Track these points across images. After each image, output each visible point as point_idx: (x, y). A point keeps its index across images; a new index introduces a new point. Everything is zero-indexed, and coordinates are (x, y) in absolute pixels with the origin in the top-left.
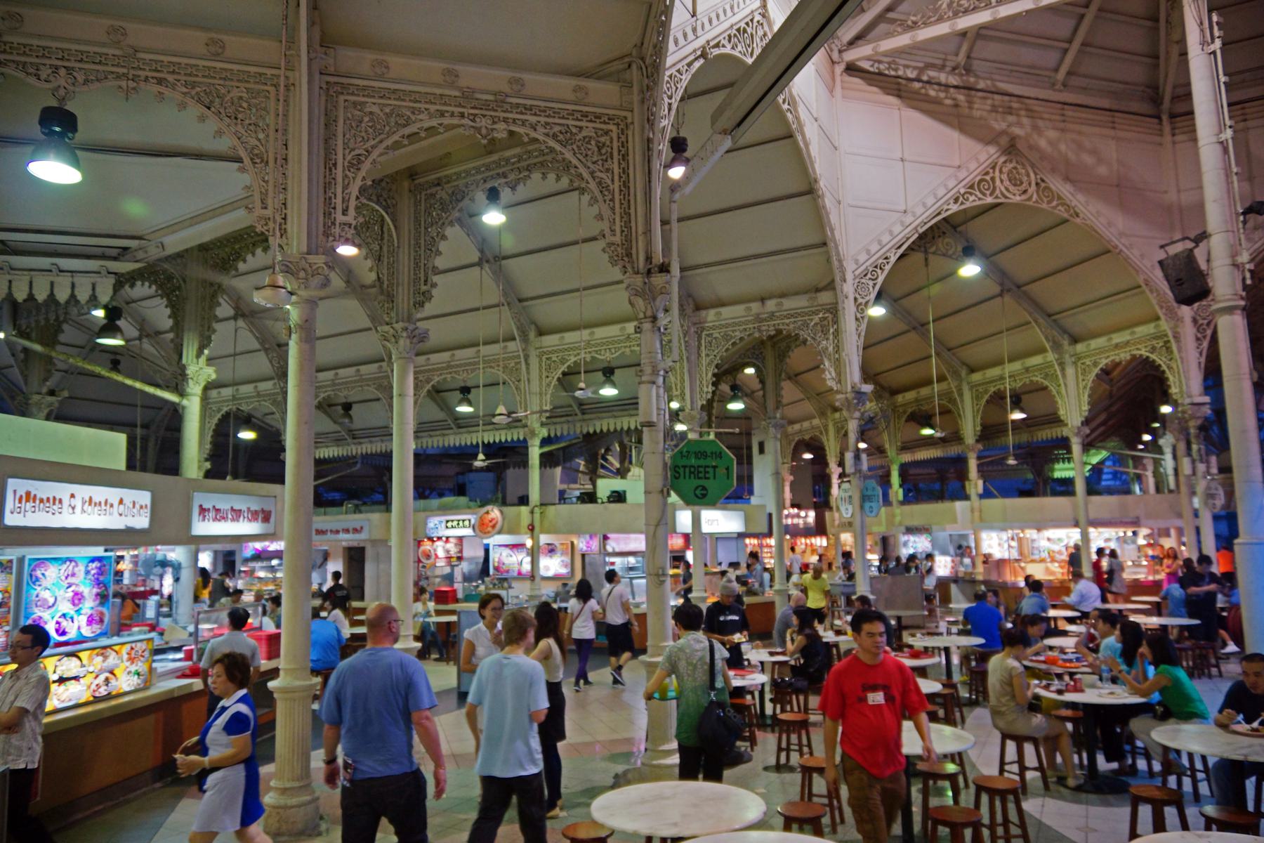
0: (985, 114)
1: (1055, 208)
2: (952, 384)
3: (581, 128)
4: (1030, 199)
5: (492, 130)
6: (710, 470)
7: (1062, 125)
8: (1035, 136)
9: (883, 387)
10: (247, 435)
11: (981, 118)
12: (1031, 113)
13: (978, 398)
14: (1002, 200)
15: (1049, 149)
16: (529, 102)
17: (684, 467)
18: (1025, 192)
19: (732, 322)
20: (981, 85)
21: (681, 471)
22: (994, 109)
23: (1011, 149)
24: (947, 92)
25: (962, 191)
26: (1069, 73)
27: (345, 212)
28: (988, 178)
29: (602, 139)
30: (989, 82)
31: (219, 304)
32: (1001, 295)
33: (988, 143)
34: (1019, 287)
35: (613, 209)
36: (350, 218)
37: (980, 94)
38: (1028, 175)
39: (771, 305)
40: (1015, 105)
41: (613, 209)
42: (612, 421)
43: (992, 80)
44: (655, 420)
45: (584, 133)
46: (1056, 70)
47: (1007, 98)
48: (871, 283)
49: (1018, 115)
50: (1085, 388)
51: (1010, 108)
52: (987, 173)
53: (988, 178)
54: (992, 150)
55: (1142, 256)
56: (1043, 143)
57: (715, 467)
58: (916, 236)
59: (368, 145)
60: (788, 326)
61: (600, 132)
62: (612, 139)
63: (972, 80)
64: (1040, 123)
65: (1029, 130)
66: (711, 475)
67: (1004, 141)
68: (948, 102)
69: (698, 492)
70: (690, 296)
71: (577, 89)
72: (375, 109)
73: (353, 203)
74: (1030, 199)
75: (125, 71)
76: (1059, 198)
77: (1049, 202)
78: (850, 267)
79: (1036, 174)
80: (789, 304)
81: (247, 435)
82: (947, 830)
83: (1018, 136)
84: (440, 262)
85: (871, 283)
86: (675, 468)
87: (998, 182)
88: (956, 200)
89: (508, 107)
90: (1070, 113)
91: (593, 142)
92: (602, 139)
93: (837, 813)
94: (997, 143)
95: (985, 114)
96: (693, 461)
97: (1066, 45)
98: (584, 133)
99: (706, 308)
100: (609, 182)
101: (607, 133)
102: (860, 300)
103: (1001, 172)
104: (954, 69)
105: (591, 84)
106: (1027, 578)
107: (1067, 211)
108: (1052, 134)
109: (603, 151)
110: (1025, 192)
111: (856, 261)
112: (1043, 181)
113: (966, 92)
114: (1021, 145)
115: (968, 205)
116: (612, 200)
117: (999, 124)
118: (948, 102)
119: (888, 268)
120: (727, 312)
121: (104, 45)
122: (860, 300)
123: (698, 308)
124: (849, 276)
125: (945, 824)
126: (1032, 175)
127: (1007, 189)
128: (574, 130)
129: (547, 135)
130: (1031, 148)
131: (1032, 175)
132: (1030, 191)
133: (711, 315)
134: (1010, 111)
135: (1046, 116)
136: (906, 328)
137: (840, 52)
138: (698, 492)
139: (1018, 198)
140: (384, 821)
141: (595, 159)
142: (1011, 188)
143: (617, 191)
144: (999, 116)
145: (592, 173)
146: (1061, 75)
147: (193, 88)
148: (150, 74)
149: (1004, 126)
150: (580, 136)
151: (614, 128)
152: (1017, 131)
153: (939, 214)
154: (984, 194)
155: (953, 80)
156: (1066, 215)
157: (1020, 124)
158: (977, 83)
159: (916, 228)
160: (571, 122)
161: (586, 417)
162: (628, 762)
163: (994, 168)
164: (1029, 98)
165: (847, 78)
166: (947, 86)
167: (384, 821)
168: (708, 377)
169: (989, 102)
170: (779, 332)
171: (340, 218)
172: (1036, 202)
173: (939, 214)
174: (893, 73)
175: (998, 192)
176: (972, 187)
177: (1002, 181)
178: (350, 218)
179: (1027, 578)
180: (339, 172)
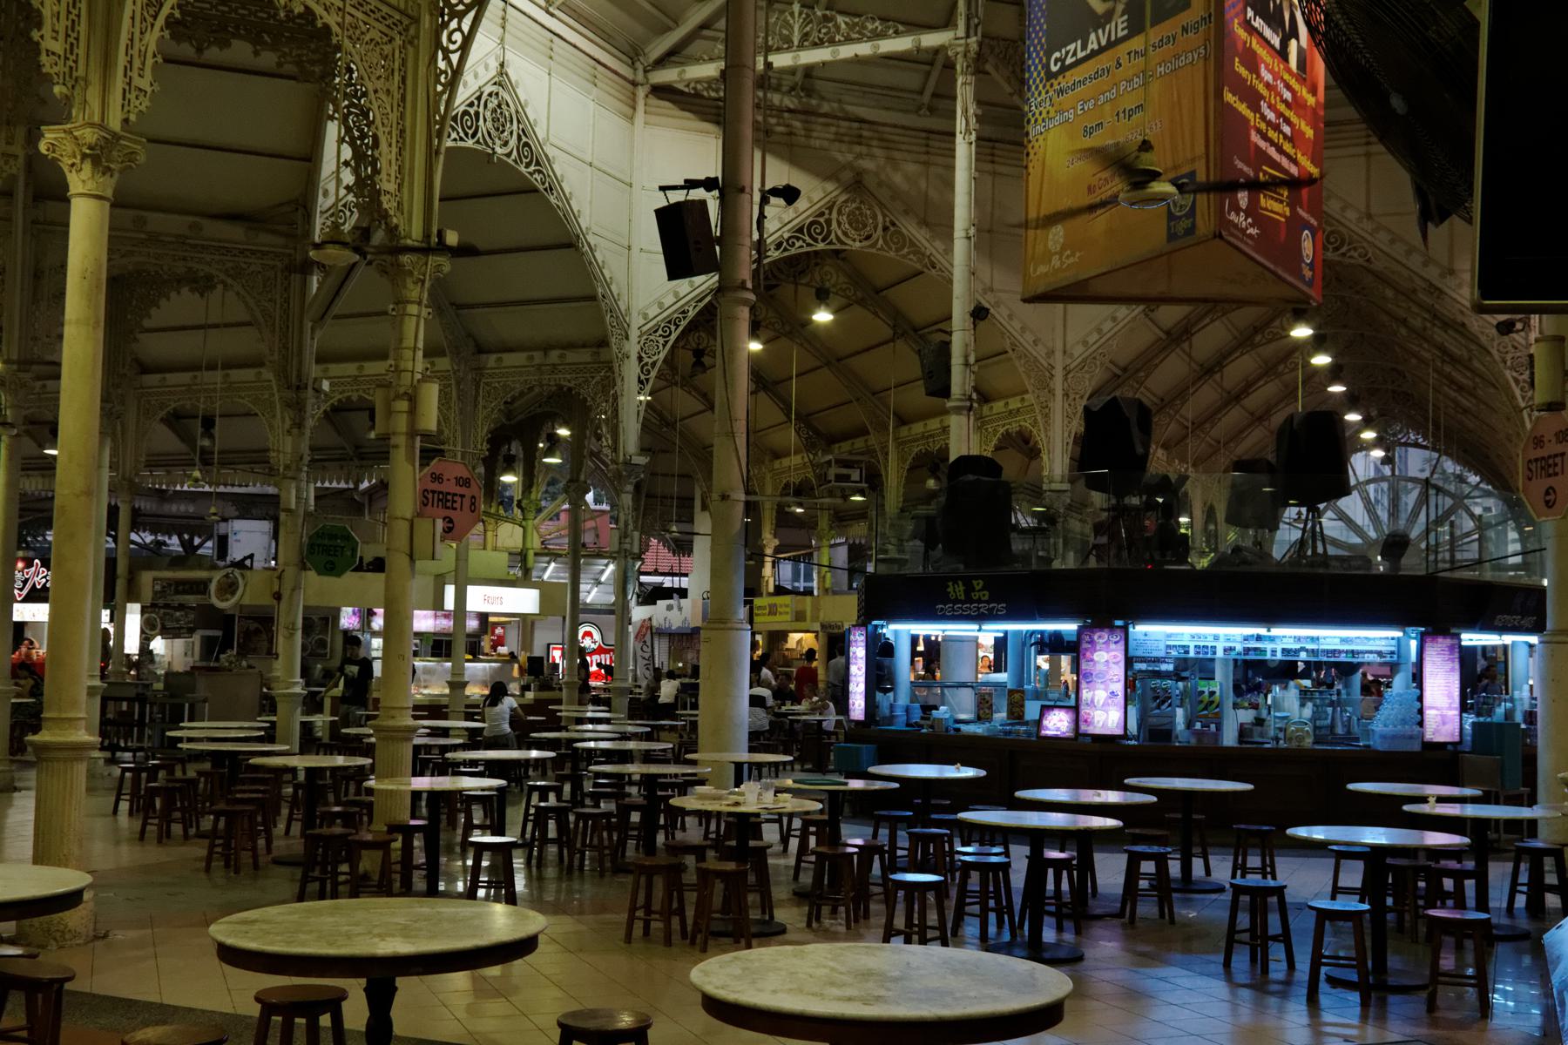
0: (826, 144)
1: (904, 256)
2: (873, 440)
4: (874, 245)
7: (924, 158)
8: (889, 169)
9: (817, 433)
11: (822, 149)
12: (887, 144)
13: (902, 459)
14: (838, 246)
15: (905, 186)
18: (868, 238)
19: (512, 370)
20: (826, 108)
22: (839, 138)
23: (857, 185)
24: (778, 117)
25: (786, 236)
26: (934, 95)
28: (822, 220)
30: (835, 105)
32: (892, 340)
33: (827, 178)
34: (916, 330)
37: (821, 120)
38: (874, 217)
39: (554, 356)
40: (865, 133)
43: (840, 101)
44: (293, 506)
46: (921, 93)
47: (856, 125)
48: (661, 341)
49: (869, 146)
51: (860, 136)
52: (822, 214)
54: (830, 186)
55: (1010, 317)
56: (898, 179)
60: (566, 379)
63: (814, 102)
64: (897, 155)
65: (882, 161)
67: (847, 176)
68: (780, 129)
70: (469, 335)
71: (192, 226)
74: (874, 245)
76: (912, 244)
77: (897, 250)
78: (636, 321)
79: (884, 216)
80: (572, 357)
83: (865, 171)
84: (147, 323)
85: (661, 341)
86: (311, 546)
87: (834, 225)
90: (937, 144)
94: (838, 180)
95: (826, 144)
96: (326, 542)
97: (927, 68)
99: (490, 352)
102: (646, 360)
103: (840, 212)
104: (793, 89)
105: (205, 222)
106: (1302, 705)
107: (920, 261)
108: (912, 168)
110: (868, 238)
111: (645, 316)
112: (894, 224)
113: (803, 117)
114: (870, 182)
115: (793, 251)
117: (843, 155)
118: (780, 129)
119: (684, 323)
120: (511, 359)
122: (646, 360)
123: (481, 350)
124: (634, 334)
126: (880, 218)
127: (845, 234)
130: (880, 184)
131: (880, 218)
132: (875, 236)
133: (491, 360)
134: (859, 140)
135: (904, 147)
136: (818, 363)
137: (646, 71)
139: (858, 244)
142: (852, 232)
144: (844, 147)
146: (926, 98)
149: (850, 157)
152: (867, 164)
154: (816, 240)
155: (789, 102)
156: (918, 266)
157: (872, 157)
158: (819, 106)
161: (364, 463)
163: (830, 209)
164: (884, 125)
165: (653, 101)
166: (781, 110)
168: (482, 431)
169: (833, 129)
170: (560, 387)
172: (882, 249)
174: (713, 94)
175: (833, 236)
176: (800, 230)
177: (839, 224)
179: (1302, 705)
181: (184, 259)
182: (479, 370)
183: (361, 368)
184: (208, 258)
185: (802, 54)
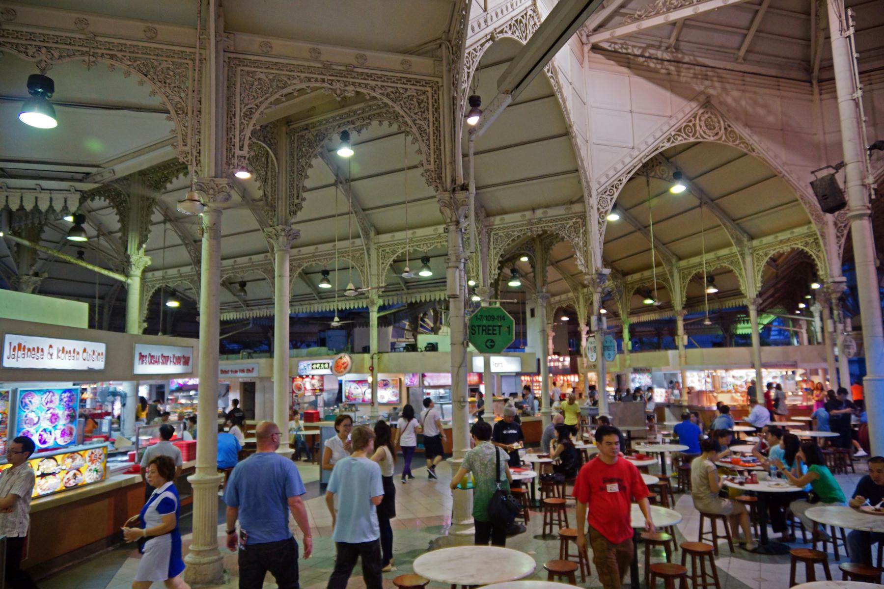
0: (689, 79)
1: (738, 145)
2: (666, 268)
3: (406, 89)
4: (720, 139)
5: (344, 91)
6: (497, 328)
7: (743, 87)
8: (724, 95)
9: (617, 271)
10: (173, 304)
11: (686, 83)
12: (721, 79)
13: (684, 278)
14: (701, 140)
15: (734, 104)
16: (370, 71)
17: (479, 326)
18: (717, 134)
19: (512, 225)
20: (686, 59)
21: (476, 329)
22: (695, 76)
23: (707, 104)
24: (662, 64)
25: (673, 133)
26: (748, 51)
27: (241, 148)
28: (691, 124)
29: (421, 97)
30: (692, 57)
31: (153, 213)
32: (700, 206)
33: (691, 100)
34: (712, 200)
35: (429, 146)
36: (245, 152)
37: (685, 66)
38: (719, 123)
39: (539, 213)
40: (710, 73)
41: (429, 146)
42: (428, 294)
43: (694, 56)
44: (458, 293)
45: (409, 93)
46: (739, 49)
47: (704, 69)
48: (609, 198)
49: (712, 81)
50: (759, 271)
51: (707, 75)
52: (690, 121)
53: (691, 124)
54: (694, 104)
55: (799, 179)
56: (729, 100)
57: (500, 326)
58: (641, 165)
59: (257, 101)
60: (551, 228)
61: (420, 93)
62: (428, 97)
63: (680, 56)
64: (728, 86)
65: (719, 90)
66: (497, 332)
67: (702, 98)
68: (663, 71)
69: (488, 344)
70: (482, 207)
72: (262, 76)
73: (247, 142)
74: (720, 139)
75: (87, 49)
76: (741, 138)
77: (734, 141)
78: (594, 186)
79: (724, 122)
80: (552, 212)
81: (173, 304)
82: (662, 580)
83: (712, 95)
84: (308, 183)
85: (609, 198)
86: (472, 327)
87: (698, 127)
88: (669, 140)
89: (355, 75)
90: (748, 79)
91: (415, 100)
92: (421, 97)
93: (585, 568)
94: (698, 100)
95: (689, 79)
96: (485, 322)
97: (745, 32)
98: (409, 93)
99: (494, 215)
100: (426, 127)
101: (424, 93)
102: (602, 210)
103: (700, 120)
104: (667, 48)
107: (746, 147)
108: (736, 94)
109: (422, 106)
110: (717, 134)
111: (599, 183)
112: (729, 126)
113: (676, 64)
114: (714, 101)
115: (677, 143)
116: (428, 140)
117: (698, 87)
118: (663, 71)
119: (621, 187)
120: (508, 218)
121: (72, 31)
122: (602, 210)
123: (488, 215)
124: (594, 193)
125: (661, 575)
126: (722, 122)
127: (704, 132)
128: (401, 91)
129: (383, 94)
130: (721, 103)
131: (722, 122)
132: (720, 133)
133: (497, 220)
134: (706, 77)
135: (732, 81)
136: (634, 229)
137: (588, 36)
138: (488, 344)
139: (712, 138)
140: (269, 574)
141: (416, 111)
142: (707, 131)
143: (431, 133)
144: (699, 81)
145: (414, 121)
146: (742, 53)
147: (135, 61)
148: (105, 52)
149: (702, 88)
150: (406, 95)
151: (429, 89)
152: (711, 91)
153: (657, 149)
154: (688, 136)
155: (667, 56)
156: (745, 150)
157: (713, 87)
158: (683, 58)
159: (640, 159)
160: (399, 85)
161: (410, 291)
162: (439, 532)
163: (695, 117)
164: (719, 68)
165: (592, 55)
166: (662, 60)
167: (269, 574)
168: (495, 263)
169: (692, 71)
170: (545, 232)
171: (238, 152)
172: (725, 141)
173: (657, 149)
174: (624, 51)
175: (698, 134)
176: (679, 131)
177: (701, 127)
178: (245, 152)
180: (237, 120)
181: (353, 84)
182: (489, 229)
183: (414, 233)
184: (373, 83)
185: (700, 6)
